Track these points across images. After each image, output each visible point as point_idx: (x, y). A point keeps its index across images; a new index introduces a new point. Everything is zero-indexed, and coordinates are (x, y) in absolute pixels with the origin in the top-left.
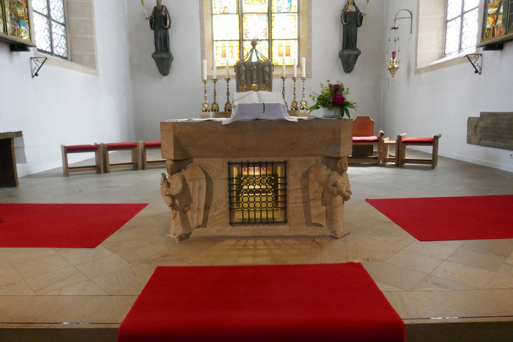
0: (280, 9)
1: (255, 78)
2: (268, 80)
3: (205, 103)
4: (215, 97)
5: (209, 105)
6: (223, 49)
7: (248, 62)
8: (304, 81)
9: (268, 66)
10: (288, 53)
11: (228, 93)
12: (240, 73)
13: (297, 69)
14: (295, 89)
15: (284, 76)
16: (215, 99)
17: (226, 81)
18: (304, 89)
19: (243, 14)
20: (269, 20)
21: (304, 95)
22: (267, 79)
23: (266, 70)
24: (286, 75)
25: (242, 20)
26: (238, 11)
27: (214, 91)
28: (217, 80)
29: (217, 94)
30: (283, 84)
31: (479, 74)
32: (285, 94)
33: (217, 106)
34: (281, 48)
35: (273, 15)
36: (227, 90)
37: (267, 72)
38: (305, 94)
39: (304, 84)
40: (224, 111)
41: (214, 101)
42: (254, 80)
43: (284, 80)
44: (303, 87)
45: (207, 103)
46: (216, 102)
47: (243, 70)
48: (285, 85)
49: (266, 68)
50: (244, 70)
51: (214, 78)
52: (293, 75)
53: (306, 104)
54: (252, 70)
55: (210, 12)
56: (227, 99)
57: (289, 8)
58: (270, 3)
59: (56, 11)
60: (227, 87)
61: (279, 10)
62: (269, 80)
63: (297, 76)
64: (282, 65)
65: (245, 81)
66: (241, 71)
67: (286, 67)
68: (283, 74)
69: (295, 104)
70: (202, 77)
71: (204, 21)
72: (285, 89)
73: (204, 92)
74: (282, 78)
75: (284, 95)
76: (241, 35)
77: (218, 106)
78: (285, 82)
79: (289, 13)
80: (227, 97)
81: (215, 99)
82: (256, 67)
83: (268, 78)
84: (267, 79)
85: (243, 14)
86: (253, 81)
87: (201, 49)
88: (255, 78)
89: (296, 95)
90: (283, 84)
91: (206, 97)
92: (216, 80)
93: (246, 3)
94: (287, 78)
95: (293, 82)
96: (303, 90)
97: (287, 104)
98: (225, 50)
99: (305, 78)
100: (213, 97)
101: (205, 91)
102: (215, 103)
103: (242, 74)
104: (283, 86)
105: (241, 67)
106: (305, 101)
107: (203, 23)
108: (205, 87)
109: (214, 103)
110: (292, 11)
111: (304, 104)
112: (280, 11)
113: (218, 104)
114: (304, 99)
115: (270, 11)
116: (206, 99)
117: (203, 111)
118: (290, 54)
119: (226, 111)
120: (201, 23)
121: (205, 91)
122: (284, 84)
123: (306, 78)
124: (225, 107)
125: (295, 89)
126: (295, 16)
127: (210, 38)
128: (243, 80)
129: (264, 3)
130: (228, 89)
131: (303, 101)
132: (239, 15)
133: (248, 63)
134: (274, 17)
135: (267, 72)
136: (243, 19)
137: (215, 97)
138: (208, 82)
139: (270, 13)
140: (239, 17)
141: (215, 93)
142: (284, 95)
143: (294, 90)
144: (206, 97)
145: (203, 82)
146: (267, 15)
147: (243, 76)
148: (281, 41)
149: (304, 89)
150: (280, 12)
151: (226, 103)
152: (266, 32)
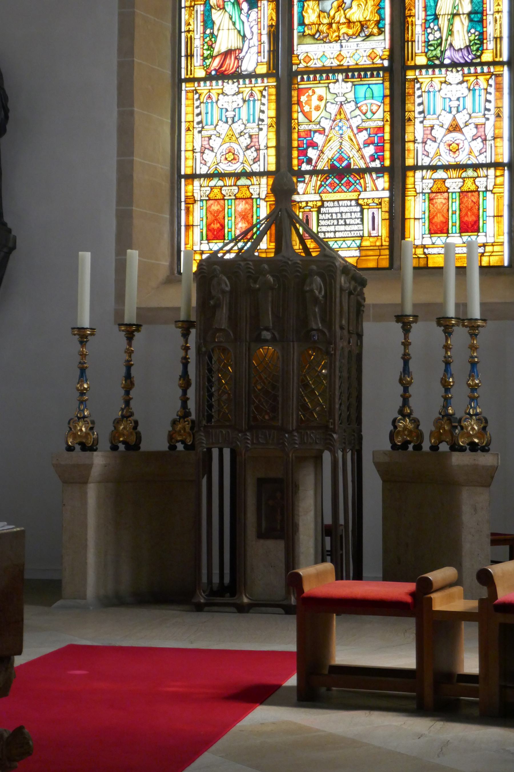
0: (438, 52)
1: (269, 319)
2: (318, 330)
3: (79, 418)
4: (127, 393)
5: (93, 422)
6: (215, 207)
7: (245, 260)
8: (473, 336)
9: (322, 276)
10: (470, 218)
11: (128, 376)
12: (212, 302)
13: (481, 280)
14: (447, 364)
15: (409, 310)
16: (127, 403)
17: (179, 332)
18: (474, 365)
19: (292, 75)
20: (392, 96)
21: (473, 388)
22: (316, 324)
23: (312, 291)
24: (415, 305)
25: (290, 97)
26: (276, 67)
27: (123, 370)
28: (138, 326)
29: (136, 381)
30: (403, 343)
31: (414, 324)
32: (410, 383)
33: (135, 428)
34: (440, 200)
35: (410, 75)
36: (180, 367)
37: (316, 300)
38: (477, 385)
39: (473, 348)
40: (163, 446)
41: (122, 410)
42: (267, 329)
43: (406, 329)
44: (472, 357)
45: (84, 417)
46: (132, 414)
47: (223, 292)
48: (411, 350)
49: (311, 284)
50: (228, 289)
51: (126, 321)
52: (443, 306)
53: (484, 428)
54: (259, 289)
55: (168, 72)
56: (179, 404)
57: (475, 48)
58: (397, 32)
59: (253, 28)
60: (182, 353)
61: (434, 53)
62: (326, 331)
63: (482, 312)
64: (442, 265)
65: (326, 331)
66: (214, 293)
67: (415, 276)
68: (402, 305)
69: (446, 428)
70: (119, 314)
71: (132, 105)
72: (411, 363)
73: (78, 372)
74: (400, 318)
75: (406, 389)
76: (284, 153)
77: (139, 428)
78: (411, 335)
79: (476, 65)
80: (180, 392)
81: (127, 403)
82: (273, 276)
83: (323, 321)
84: (315, 327)
85: (292, 75)
86: (260, 335)
87: (117, 210)
88: (269, 319)
89: (452, 390)
90: (403, 343)
91: (82, 394)
92: (134, 328)
93: (304, 36)
94: (419, 318)
95: (443, 335)
96: (472, 371)
97: (418, 425)
98: (218, 212)
99: (480, 323)
100: (122, 392)
101: (83, 371)
102: (127, 415)
103: (217, 306)
104: (402, 352)
105: (215, 281)
106: (476, 414)
107: (132, 113)
108: (83, 355)
109: (123, 416)
110: (487, 57)
111: (473, 429)
112: (438, 58)
113: (136, 423)
114: (475, 408)
115: (397, 57)
116: (472, 399)
117: (70, 449)
118: (477, 222)
119: (172, 447)
120: (121, 114)
121: (83, 371)
122: (406, 344)
123: (484, 320)
124: (391, 432)
125: (447, 364)
126: (497, 76)
127: (166, 167)
128: (220, 330)
129: (375, 31)
130: (129, 367)
131: (469, 414)
132: (278, 80)
133: (242, 263)
134: (416, 80)
135: (318, 298)
136: (294, 93)
137: (127, 393)
138: (91, 335)
139: (397, 66)
140: (278, 88)
141: (128, 376)
142: (406, 389)
143: (446, 370)
144: (82, 394)
145: (177, 327)
146: (387, 75)
147: (224, 313)
148: (441, 174)
149: (474, 365)
150: (437, 62)
151: (175, 417)
152: (382, 139)
